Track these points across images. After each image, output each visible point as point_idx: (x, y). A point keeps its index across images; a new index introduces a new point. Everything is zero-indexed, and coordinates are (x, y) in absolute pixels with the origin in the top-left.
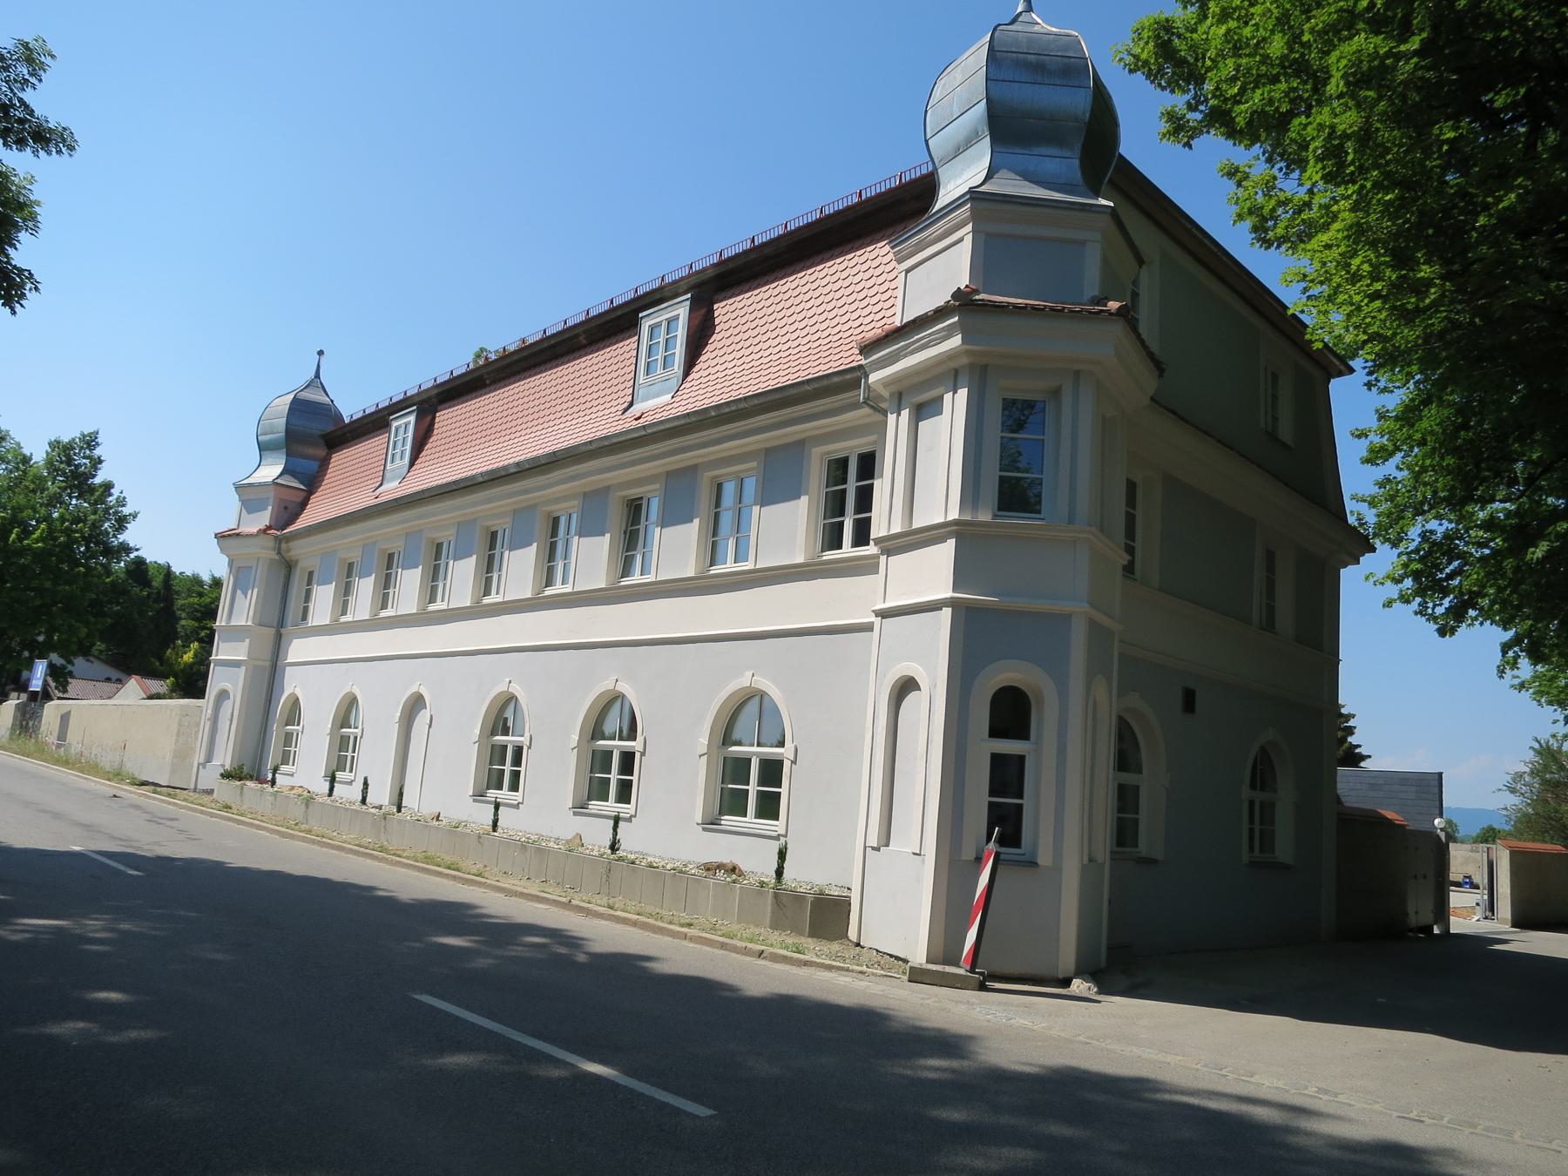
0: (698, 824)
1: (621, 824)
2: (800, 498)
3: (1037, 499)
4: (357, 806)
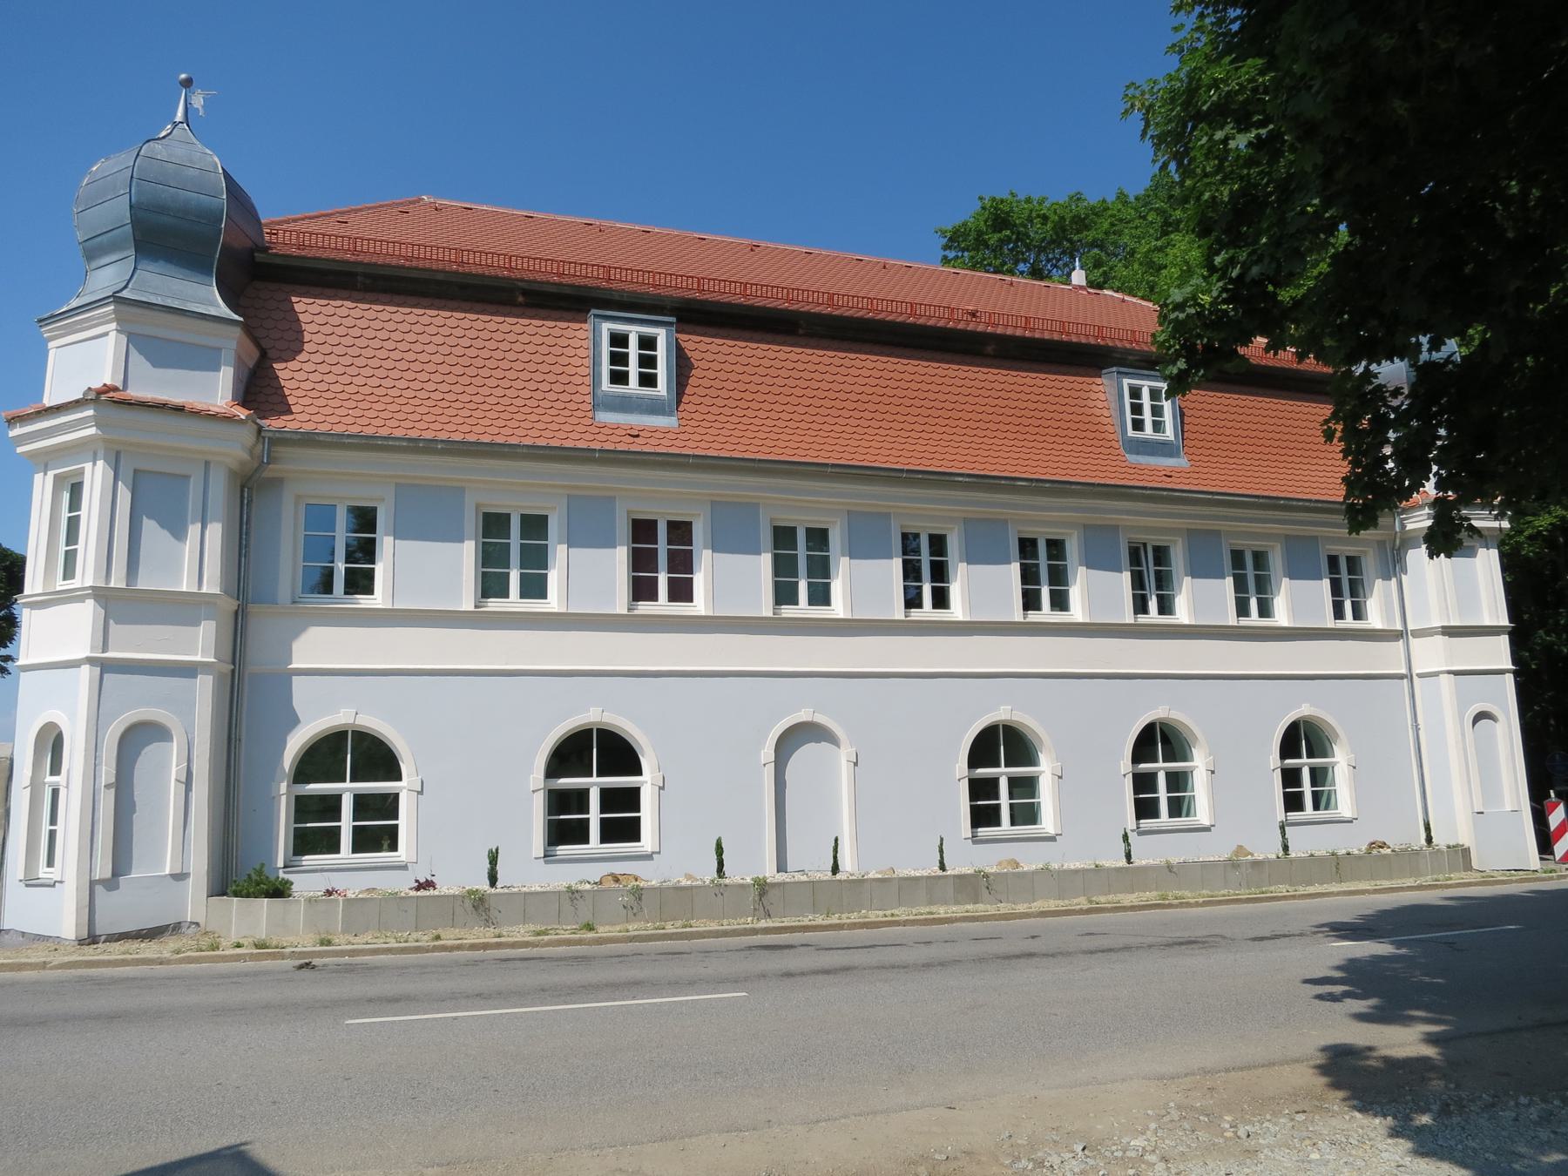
0: (21, 881)
1: (1287, 828)
2: (463, 542)
3: (918, 591)
4: (940, 873)
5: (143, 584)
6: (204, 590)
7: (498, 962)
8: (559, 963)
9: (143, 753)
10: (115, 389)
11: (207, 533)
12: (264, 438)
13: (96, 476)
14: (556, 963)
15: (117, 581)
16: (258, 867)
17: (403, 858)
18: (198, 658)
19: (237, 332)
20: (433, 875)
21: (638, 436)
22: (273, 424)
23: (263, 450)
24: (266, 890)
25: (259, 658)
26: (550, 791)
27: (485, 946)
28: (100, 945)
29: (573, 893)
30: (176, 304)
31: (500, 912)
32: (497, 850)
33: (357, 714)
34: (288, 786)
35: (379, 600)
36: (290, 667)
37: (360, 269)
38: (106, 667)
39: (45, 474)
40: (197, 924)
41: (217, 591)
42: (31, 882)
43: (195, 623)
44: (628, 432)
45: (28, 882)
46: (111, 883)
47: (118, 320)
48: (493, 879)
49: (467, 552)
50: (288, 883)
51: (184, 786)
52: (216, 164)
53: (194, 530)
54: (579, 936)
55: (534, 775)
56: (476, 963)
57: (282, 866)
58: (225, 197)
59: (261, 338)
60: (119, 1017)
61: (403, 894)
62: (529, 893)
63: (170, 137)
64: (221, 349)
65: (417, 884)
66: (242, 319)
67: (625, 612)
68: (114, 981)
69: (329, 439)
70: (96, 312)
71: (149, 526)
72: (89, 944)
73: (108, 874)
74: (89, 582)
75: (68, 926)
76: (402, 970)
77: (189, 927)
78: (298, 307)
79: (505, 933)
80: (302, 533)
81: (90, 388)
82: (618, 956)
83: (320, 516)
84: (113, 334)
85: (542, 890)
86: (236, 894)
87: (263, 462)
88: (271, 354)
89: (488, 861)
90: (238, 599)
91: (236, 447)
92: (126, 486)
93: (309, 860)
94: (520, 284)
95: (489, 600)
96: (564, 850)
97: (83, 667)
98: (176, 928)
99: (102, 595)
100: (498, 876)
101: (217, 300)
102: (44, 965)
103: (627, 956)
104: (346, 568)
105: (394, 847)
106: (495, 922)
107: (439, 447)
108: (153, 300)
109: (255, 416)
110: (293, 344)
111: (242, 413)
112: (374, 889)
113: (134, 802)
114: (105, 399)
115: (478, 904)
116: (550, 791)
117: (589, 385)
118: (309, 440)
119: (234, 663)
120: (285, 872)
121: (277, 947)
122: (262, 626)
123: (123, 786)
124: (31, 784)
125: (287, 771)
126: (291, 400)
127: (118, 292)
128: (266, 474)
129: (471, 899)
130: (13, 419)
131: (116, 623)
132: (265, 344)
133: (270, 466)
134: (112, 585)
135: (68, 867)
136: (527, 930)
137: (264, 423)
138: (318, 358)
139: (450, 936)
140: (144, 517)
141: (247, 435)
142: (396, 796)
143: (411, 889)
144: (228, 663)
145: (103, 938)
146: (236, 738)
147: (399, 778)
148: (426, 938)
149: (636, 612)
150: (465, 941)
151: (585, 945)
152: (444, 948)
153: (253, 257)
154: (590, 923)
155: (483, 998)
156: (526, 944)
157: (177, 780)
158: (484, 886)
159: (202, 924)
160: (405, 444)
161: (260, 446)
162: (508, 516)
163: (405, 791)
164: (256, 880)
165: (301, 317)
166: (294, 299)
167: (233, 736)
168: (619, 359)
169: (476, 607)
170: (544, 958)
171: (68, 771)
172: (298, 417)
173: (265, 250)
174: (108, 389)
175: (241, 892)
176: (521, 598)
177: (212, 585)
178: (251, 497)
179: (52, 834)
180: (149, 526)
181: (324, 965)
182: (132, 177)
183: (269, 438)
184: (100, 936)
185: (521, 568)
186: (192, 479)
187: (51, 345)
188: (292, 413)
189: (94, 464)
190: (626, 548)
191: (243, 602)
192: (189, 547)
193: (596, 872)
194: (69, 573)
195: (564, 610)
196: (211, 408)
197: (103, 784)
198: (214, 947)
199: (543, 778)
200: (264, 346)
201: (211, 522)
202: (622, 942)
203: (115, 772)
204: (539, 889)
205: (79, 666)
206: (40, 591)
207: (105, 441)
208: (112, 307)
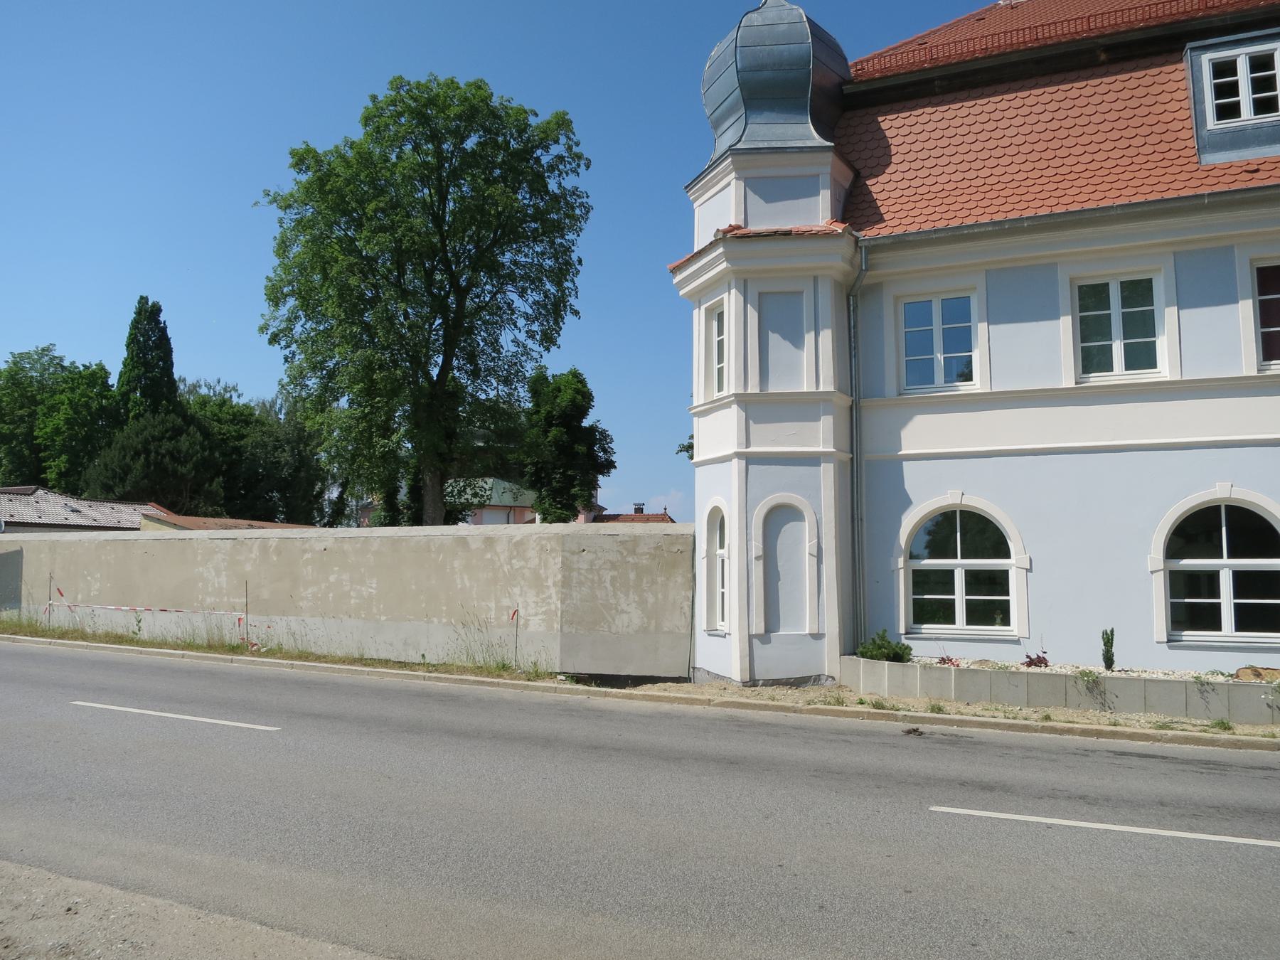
0: (705, 631)
5: (773, 388)
6: (821, 389)
7: (1111, 755)
8: (1185, 767)
9: (783, 530)
10: (738, 227)
11: (820, 339)
12: (861, 248)
13: (731, 301)
14: (1181, 767)
15: (753, 388)
16: (881, 633)
17: (1015, 633)
18: (820, 449)
19: (830, 157)
20: (1045, 653)
21: (1257, 171)
22: (869, 233)
23: (861, 259)
24: (887, 654)
25: (873, 448)
26: (1171, 572)
27: (1099, 734)
28: (757, 688)
29: (1202, 686)
30: (779, 145)
31: (1117, 697)
32: (1112, 631)
33: (963, 494)
34: (905, 561)
35: (978, 386)
36: (900, 453)
37: (936, 74)
38: (750, 460)
39: (700, 309)
40: (833, 678)
41: (831, 389)
42: (712, 632)
43: (816, 419)
44: (1244, 168)
45: (711, 632)
46: (765, 638)
47: (736, 169)
48: (1109, 662)
49: (1063, 329)
50: (909, 648)
51: (816, 559)
52: (801, 14)
53: (809, 338)
54: (1211, 735)
55: (1152, 555)
56: (1086, 753)
57: (904, 632)
58: (810, 40)
59: (853, 161)
60: (737, 763)
61: (1013, 669)
62: (1148, 680)
63: (765, 6)
64: (818, 175)
65: (1028, 660)
66: (833, 144)
67: (1254, 373)
68: (752, 724)
69: (918, 238)
70: (719, 169)
71: (774, 339)
72: (750, 687)
73: (761, 630)
74: (732, 391)
75: (734, 670)
76: (1006, 749)
77: (827, 680)
78: (884, 126)
79: (1121, 721)
80: (902, 331)
81: (718, 230)
82: (1263, 768)
83: (917, 313)
84: (733, 182)
85: (1165, 678)
86: (863, 655)
87: (862, 270)
88: (863, 173)
89: (1102, 643)
90: (852, 396)
91: (836, 261)
92: (753, 307)
93: (928, 628)
94: (1100, 41)
95: (1090, 375)
96: (1189, 635)
97: (733, 460)
98: (816, 680)
99: (743, 400)
100: (1115, 658)
101: (812, 133)
102: (709, 702)
103: (1275, 769)
104: (944, 358)
105: (1006, 621)
106: (1111, 706)
107: (1026, 225)
108: (761, 145)
109: (850, 228)
110: (881, 158)
111: (839, 228)
112: (986, 661)
113: (778, 572)
114: (732, 237)
115: (1093, 686)
116: (1171, 572)
117: (1194, 147)
118: (900, 242)
119: (852, 453)
120: (906, 638)
121: (891, 709)
122: (874, 419)
123: (769, 557)
124: (707, 556)
125: (903, 547)
126: (883, 210)
127: (732, 146)
128: (866, 281)
129: (1083, 680)
130: (674, 269)
131: (755, 423)
132: (858, 165)
133: (868, 273)
134: (749, 391)
135: (732, 623)
136: (1149, 720)
137: (861, 234)
138: (905, 166)
139: (1060, 717)
140: (770, 332)
141: (846, 247)
142: (1006, 572)
143: (1022, 664)
144: (846, 452)
145: (761, 682)
146: (858, 518)
147: (1007, 555)
148: (1035, 716)
149: (1268, 373)
150: (1077, 726)
151: (1218, 746)
152: (1053, 730)
153: (842, 90)
154: (1225, 721)
155: (1087, 802)
156: (1146, 737)
157: (810, 554)
158: (1099, 667)
159: (837, 677)
160: (990, 229)
161: (858, 256)
162: (1107, 285)
163: (1014, 568)
164: (878, 645)
165: (888, 134)
166: (880, 119)
167: (856, 516)
168: (1227, 90)
169: (1076, 383)
170: (1167, 758)
171: (729, 545)
172: (890, 223)
173: (851, 82)
174: (733, 228)
175: (866, 653)
176: (1126, 369)
177: (827, 385)
178: (856, 303)
179: (723, 593)
180: (774, 339)
181: (932, 733)
182: (736, 47)
183: (866, 247)
184: (759, 680)
185: (1124, 339)
186: (804, 294)
187: (696, 205)
188: (885, 221)
189: (730, 294)
190: (1250, 301)
191: (856, 398)
192: (807, 354)
193: (1233, 662)
194: (720, 389)
195: (1178, 378)
196: (814, 229)
197: (754, 556)
198: (840, 702)
199: (1162, 558)
200: (857, 168)
201: (822, 329)
202: (1266, 749)
203: (762, 546)
204: (1161, 677)
205: (731, 460)
206: (703, 403)
207: (735, 272)
208: (730, 159)
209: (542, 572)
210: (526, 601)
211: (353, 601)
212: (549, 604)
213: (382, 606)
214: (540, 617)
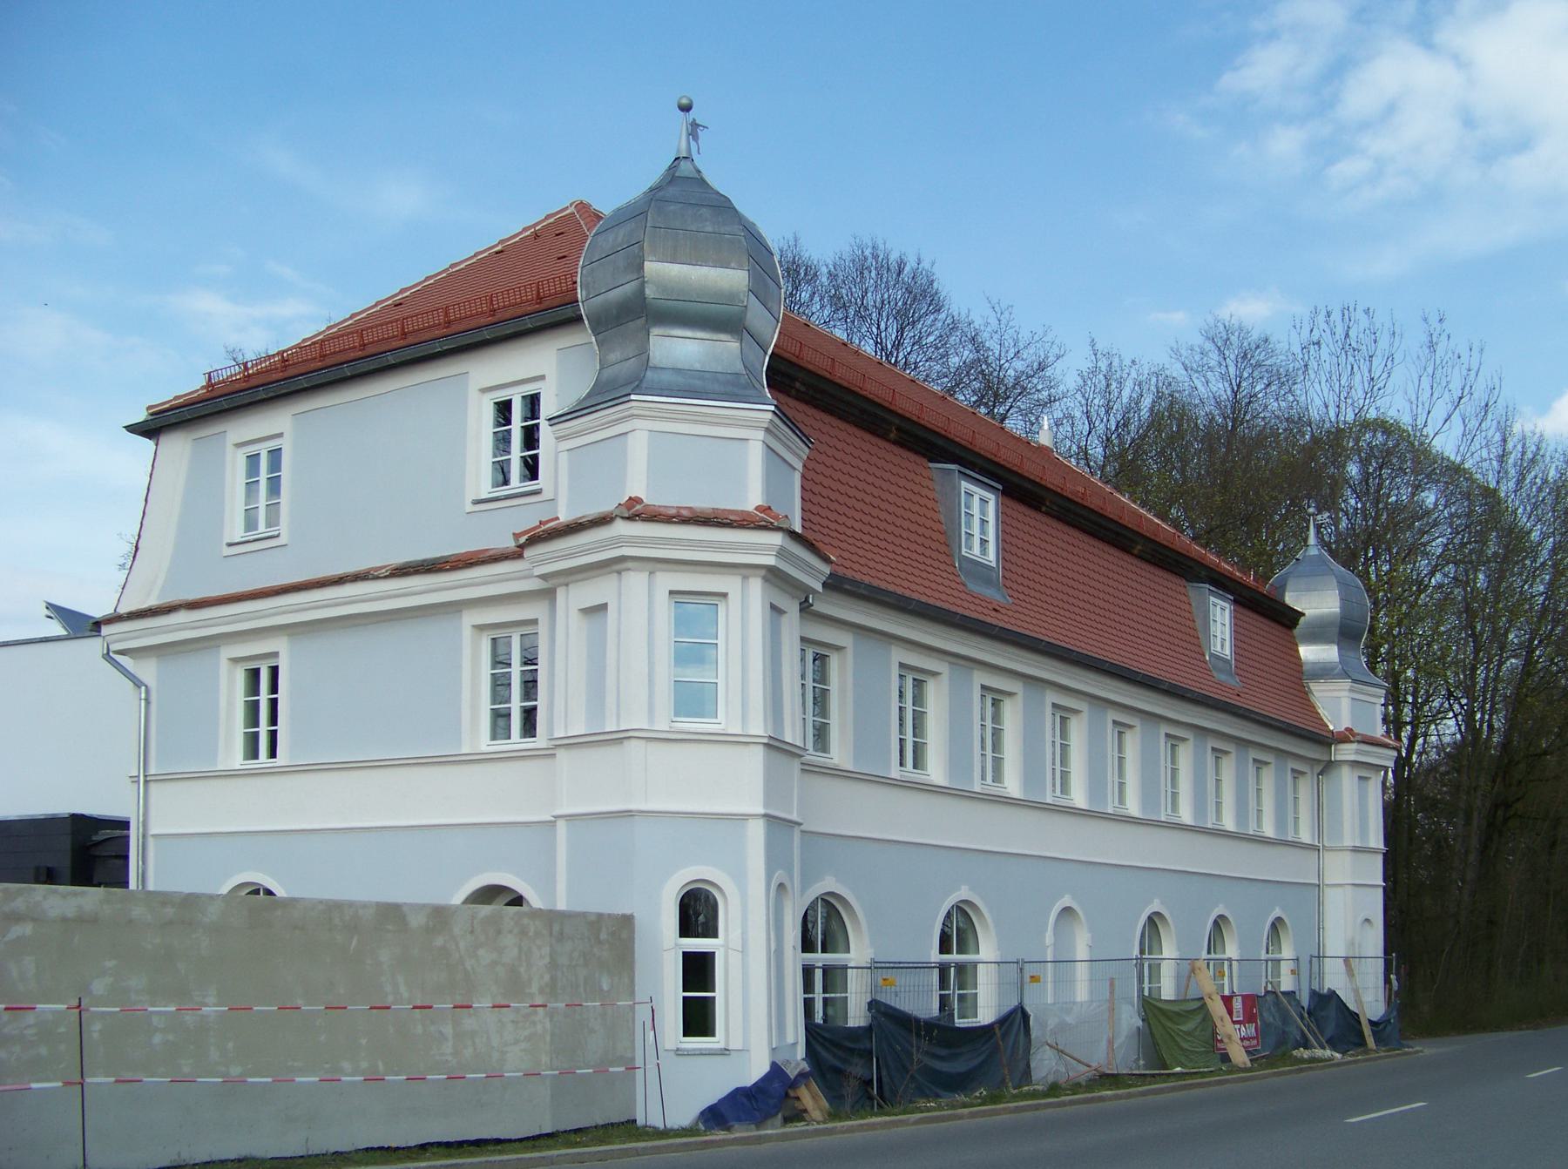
209: (522, 970)
210: (500, 1021)
211: (157, 1039)
212: (534, 1023)
213: (230, 1045)
214: (523, 1045)
